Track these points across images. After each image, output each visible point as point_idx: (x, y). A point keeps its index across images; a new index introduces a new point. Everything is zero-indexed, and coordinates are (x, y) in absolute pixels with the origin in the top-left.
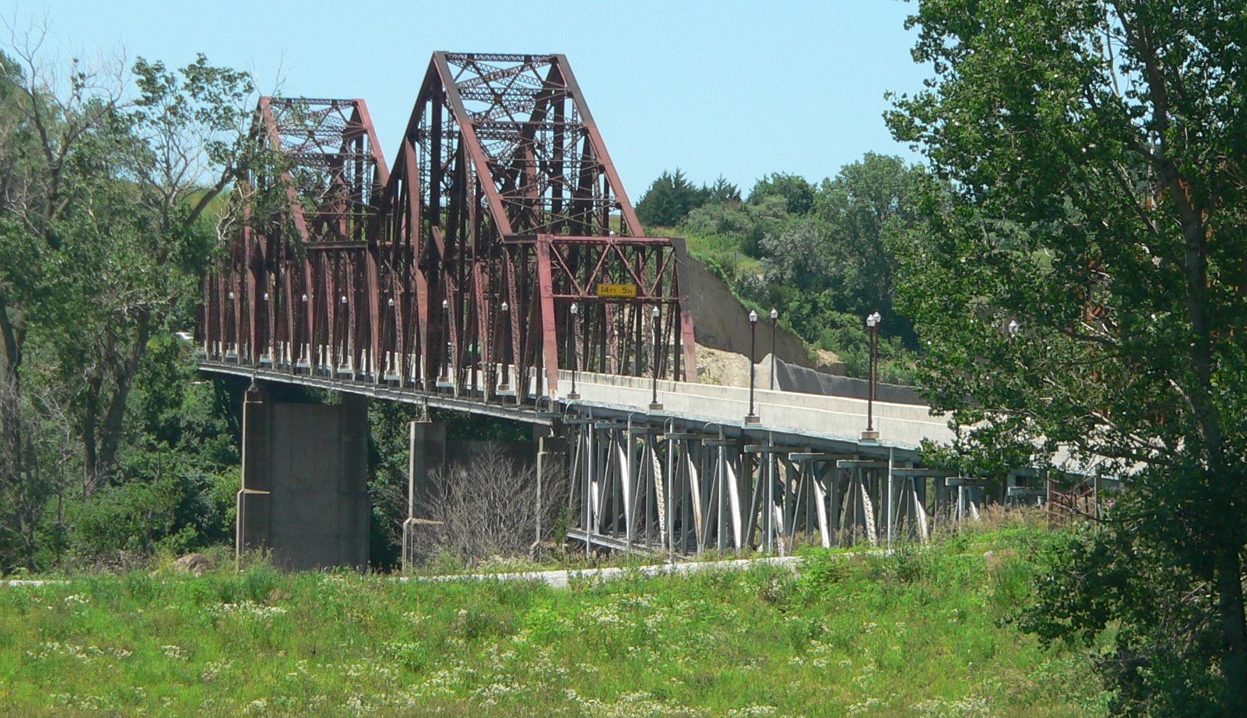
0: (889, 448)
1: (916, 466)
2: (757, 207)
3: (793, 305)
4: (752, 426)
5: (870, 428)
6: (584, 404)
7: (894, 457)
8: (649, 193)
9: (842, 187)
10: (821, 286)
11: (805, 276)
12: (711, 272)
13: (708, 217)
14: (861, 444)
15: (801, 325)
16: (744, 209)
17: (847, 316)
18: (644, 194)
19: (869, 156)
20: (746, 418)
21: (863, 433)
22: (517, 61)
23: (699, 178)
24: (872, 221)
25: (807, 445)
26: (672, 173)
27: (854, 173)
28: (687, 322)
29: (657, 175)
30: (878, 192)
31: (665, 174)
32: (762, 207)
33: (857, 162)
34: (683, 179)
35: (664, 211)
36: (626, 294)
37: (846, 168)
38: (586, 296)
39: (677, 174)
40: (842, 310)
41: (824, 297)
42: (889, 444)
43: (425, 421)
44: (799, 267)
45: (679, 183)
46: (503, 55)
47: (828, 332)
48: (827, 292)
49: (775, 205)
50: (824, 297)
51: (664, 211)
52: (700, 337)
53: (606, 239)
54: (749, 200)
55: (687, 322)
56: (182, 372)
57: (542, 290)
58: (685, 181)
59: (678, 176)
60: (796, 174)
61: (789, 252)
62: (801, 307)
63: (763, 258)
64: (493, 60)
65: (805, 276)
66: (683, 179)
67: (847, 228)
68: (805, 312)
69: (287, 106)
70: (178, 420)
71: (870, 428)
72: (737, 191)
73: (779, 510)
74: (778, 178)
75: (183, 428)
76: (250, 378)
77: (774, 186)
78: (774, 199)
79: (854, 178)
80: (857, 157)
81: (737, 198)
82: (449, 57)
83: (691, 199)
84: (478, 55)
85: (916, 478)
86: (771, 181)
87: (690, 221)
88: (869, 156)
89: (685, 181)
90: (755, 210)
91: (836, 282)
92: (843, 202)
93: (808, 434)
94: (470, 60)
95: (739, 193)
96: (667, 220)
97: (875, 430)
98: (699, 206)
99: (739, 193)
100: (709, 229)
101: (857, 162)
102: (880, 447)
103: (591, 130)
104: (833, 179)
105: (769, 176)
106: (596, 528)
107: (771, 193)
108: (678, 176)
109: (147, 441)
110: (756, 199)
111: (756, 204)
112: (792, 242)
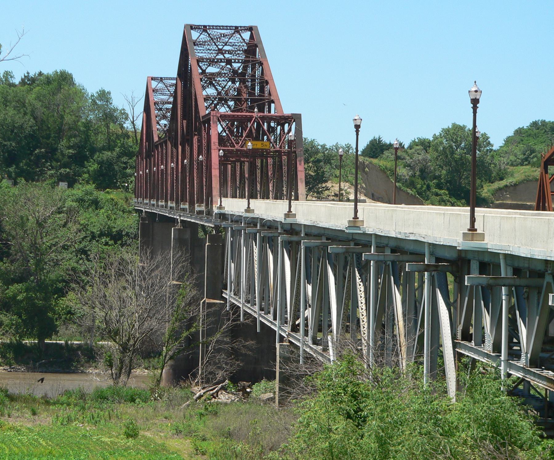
0: (371, 235)
1: (393, 251)
2: (411, 151)
3: (419, 186)
4: (290, 220)
5: (356, 217)
6: (226, 213)
7: (376, 243)
8: (368, 145)
9: (441, 138)
10: (432, 179)
11: (424, 173)
12: (381, 170)
13: (390, 154)
14: (347, 231)
15: (422, 195)
16: (406, 152)
17: (443, 191)
18: (366, 145)
19: (454, 125)
20: (285, 214)
21: (349, 221)
22: (231, 29)
23: (387, 139)
24: (453, 151)
25: (323, 235)
26: (377, 137)
27: (446, 132)
28: (300, 164)
29: (371, 138)
30: (456, 139)
31: (374, 137)
32: (413, 150)
33: (449, 127)
34: (381, 139)
35: (374, 152)
36: (264, 147)
37: (443, 129)
38: (239, 148)
39: (379, 138)
40: (441, 188)
41: (432, 183)
42: (370, 231)
43: (179, 228)
44: (422, 171)
45: (380, 141)
46: (223, 26)
47: (434, 197)
48: (434, 181)
49: (418, 150)
50: (432, 183)
51: (374, 152)
52: (375, 197)
53: (253, 114)
54: (408, 148)
55: (300, 164)
56: (128, 209)
57: (212, 144)
58: (382, 141)
59: (379, 138)
60: (427, 138)
61: (417, 164)
62: (422, 187)
63: (406, 168)
64: (217, 29)
65: (424, 173)
66: (381, 139)
67: (443, 154)
68: (424, 189)
69: (161, 81)
70: (122, 231)
71: (356, 217)
72: (403, 144)
73: (309, 288)
74: (420, 139)
75: (124, 235)
76: (142, 210)
77: (418, 142)
78: (418, 147)
79: (447, 133)
80: (448, 124)
81: (403, 147)
82: (192, 27)
83: (384, 147)
84: (209, 26)
85: (393, 262)
86: (417, 141)
87: (384, 156)
88: (454, 125)
89: (382, 141)
90: (410, 151)
91: (438, 177)
92: (441, 143)
93: (321, 225)
94: (205, 29)
95: (404, 145)
96: (374, 156)
97: (360, 219)
98: (388, 149)
99: (404, 145)
100: (391, 159)
101: (449, 127)
102: (364, 234)
103: (264, 63)
104: (438, 134)
105: (416, 138)
106: (232, 293)
107: (417, 145)
108: (379, 138)
109: (106, 240)
110: (410, 147)
111: (411, 149)
112: (419, 160)
